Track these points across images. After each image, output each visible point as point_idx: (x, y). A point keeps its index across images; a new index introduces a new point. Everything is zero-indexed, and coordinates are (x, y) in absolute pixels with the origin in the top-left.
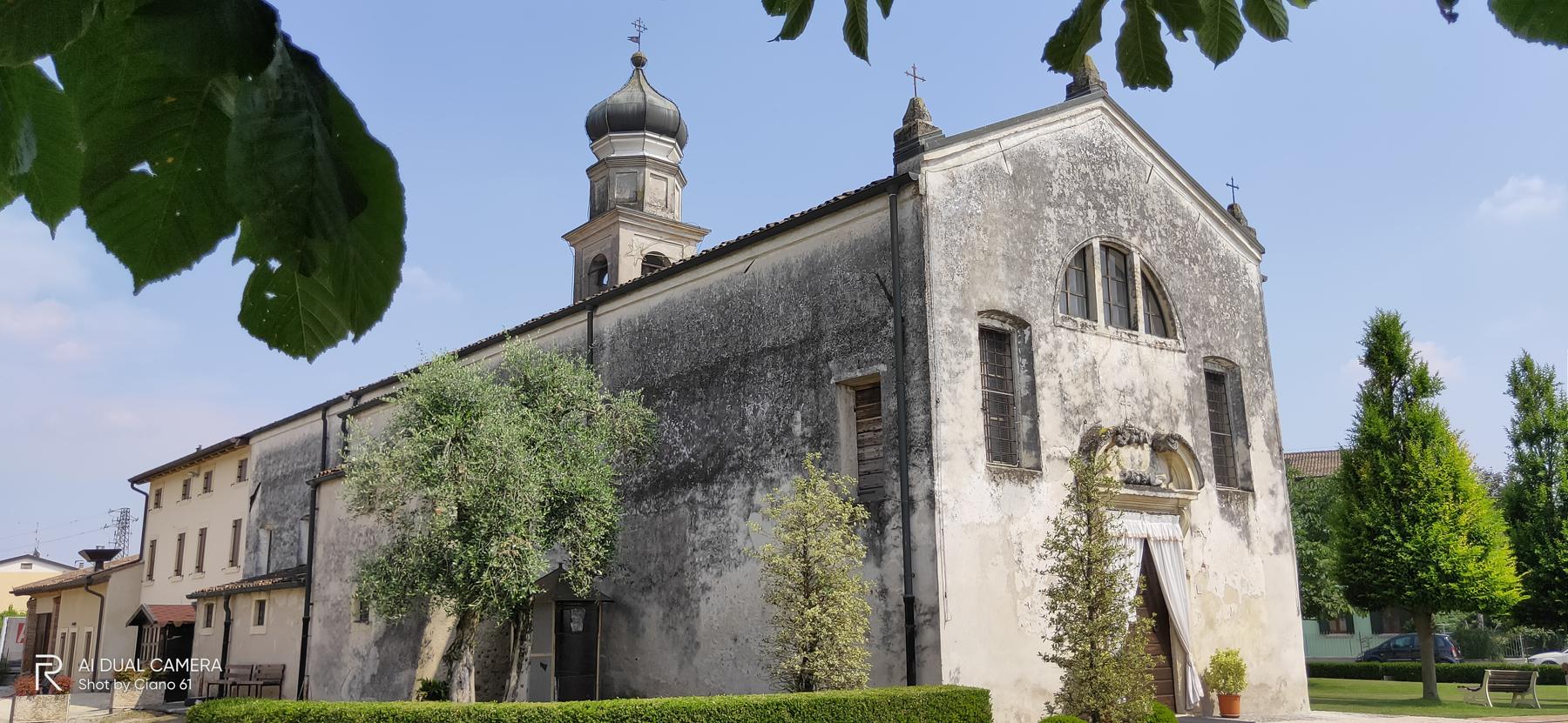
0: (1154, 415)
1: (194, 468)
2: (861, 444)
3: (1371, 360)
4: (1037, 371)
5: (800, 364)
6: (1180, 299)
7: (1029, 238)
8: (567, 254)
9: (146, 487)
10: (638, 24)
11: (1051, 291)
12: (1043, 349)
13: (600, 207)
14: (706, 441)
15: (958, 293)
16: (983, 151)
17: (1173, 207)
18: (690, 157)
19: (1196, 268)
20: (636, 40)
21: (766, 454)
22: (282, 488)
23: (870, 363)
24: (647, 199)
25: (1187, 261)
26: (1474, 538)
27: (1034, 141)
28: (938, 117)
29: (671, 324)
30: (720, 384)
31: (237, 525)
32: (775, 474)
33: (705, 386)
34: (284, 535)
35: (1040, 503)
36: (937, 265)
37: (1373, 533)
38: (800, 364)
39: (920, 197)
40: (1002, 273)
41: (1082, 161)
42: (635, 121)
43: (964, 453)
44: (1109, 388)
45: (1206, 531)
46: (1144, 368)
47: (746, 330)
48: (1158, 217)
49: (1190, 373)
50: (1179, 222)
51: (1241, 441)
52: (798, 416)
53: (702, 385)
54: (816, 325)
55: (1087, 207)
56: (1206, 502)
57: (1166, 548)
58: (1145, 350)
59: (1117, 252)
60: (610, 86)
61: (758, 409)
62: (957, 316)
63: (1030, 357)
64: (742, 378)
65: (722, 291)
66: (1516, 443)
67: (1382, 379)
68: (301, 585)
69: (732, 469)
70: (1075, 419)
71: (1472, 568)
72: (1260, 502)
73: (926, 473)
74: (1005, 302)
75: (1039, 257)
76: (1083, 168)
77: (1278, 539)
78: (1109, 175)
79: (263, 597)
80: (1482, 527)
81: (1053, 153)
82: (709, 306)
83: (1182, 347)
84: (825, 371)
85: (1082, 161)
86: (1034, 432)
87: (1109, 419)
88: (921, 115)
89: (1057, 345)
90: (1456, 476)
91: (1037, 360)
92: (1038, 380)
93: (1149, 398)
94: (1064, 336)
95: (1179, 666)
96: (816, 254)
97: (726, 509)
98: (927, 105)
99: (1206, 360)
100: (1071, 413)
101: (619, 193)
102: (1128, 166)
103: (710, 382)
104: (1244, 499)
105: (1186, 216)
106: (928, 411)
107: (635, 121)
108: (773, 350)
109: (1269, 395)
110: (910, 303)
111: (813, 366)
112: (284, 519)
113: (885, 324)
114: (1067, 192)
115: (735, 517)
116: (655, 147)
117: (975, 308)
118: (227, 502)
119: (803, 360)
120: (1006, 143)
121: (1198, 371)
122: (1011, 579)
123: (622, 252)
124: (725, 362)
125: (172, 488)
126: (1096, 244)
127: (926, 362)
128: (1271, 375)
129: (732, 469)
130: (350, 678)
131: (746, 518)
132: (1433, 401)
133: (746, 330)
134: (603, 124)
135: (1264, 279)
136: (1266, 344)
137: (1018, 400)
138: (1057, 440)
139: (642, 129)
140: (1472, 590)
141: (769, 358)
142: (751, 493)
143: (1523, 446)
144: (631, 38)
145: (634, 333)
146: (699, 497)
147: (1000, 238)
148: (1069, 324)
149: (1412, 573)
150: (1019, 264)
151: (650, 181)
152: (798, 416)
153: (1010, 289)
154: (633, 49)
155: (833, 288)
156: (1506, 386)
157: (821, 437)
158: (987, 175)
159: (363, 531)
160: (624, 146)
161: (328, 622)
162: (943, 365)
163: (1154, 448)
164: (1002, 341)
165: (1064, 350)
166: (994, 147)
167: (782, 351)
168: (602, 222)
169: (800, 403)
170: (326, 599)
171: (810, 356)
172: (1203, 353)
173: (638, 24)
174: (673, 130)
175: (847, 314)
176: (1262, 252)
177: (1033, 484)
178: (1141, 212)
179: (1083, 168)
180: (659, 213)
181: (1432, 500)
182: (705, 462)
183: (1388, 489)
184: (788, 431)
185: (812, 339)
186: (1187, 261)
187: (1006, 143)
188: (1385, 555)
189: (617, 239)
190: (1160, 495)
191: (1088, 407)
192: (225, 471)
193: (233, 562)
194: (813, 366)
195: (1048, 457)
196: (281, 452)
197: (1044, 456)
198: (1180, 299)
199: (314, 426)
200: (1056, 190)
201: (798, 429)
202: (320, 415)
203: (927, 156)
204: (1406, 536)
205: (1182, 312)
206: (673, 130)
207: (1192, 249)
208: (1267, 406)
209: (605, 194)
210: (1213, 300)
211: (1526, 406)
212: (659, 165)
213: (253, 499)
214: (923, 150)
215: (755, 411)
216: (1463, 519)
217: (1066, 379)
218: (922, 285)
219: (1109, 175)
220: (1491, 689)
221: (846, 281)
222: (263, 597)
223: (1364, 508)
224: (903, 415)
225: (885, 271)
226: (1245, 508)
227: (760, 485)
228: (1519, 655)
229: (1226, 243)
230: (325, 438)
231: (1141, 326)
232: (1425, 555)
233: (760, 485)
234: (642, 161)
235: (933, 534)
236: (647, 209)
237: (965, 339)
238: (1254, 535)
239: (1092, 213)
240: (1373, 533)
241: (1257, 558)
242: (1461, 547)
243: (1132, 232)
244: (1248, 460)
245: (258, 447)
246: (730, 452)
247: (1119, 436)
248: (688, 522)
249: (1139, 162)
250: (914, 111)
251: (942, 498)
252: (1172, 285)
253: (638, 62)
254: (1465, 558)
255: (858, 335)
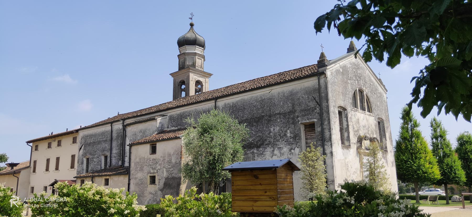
1: (53, 139)
2: (306, 139)
3: (403, 118)
5: (289, 118)
7: (345, 88)
8: (171, 79)
9: (31, 144)
10: (192, 14)
12: (349, 116)
13: (182, 67)
14: (257, 137)
16: (336, 66)
17: (370, 80)
18: (207, 52)
20: (191, 19)
21: (278, 141)
22: (93, 146)
23: (312, 119)
24: (196, 65)
26: (430, 163)
28: (328, 57)
29: (244, 105)
30: (262, 122)
31: (73, 157)
32: (281, 146)
33: (257, 122)
34: (94, 160)
36: (330, 95)
37: (406, 162)
38: (289, 118)
39: (326, 77)
40: (341, 97)
42: (194, 42)
46: (367, 121)
47: (270, 109)
49: (375, 122)
50: (372, 84)
52: (289, 131)
53: (255, 122)
54: (293, 108)
58: (367, 116)
59: (361, 92)
60: (183, 31)
61: (275, 129)
63: (347, 118)
64: (269, 121)
65: (261, 97)
66: (432, 139)
67: (406, 123)
68: (127, 174)
69: (266, 144)
70: (356, 133)
71: (430, 171)
73: (330, 147)
74: (342, 105)
76: (354, 70)
78: (359, 72)
79: (107, 177)
80: (431, 160)
82: (256, 101)
84: (297, 120)
86: (348, 137)
87: (362, 134)
88: (325, 57)
89: (352, 115)
90: (425, 147)
91: (349, 118)
94: (353, 113)
96: (293, 90)
97: (265, 155)
98: (326, 54)
101: (188, 63)
103: (258, 121)
104: (386, 153)
105: (373, 82)
106: (330, 131)
107: (194, 42)
108: (279, 114)
110: (324, 104)
111: (293, 119)
112: (94, 155)
113: (316, 109)
115: (268, 157)
116: (198, 50)
117: (337, 106)
118: (69, 149)
119: (289, 117)
120: (341, 64)
122: (346, 173)
123: (190, 80)
124: (263, 116)
125: (43, 146)
127: (329, 119)
129: (266, 144)
130: (148, 200)
131: (272, 157)
132: (418, 129)
133: (270, 109)
134: (182, 43)
137: (344, 129)
138: (354, 140)
139: (195, 45)
140: (430, 176)
141: (278, 116)
142: (273, 151)
143: (434, 140)
145: (231, 107)
146: (255, 151)
148: (353, 110)
149: (416, 172)
150: (344, 94)
151: (197, 60)
152: (289, 131)
154: (190, 21)
155: (299, 99)
156: (430, 125)
157: (296, 137)
158: (338, 71)
159: (151, 159)
160: (189, 49)
161: (137, 184)
163: (370, 141)
167: (284, 114)
168: (183, 71)
169: (289, 128)
170: (136, 178)
171: (292, 116)
173: (192, 14)
174: (202, 45)
175: (304, 106)
178: (365, 81)
179: (354, 70)
180: (199, 69)
181: (420, 154)
182: (257, 142)
183: (409, 151)
184: (285, 135)
185: (293, 112)
188: (409, 167)
189: (189, 76)
191: (358, 131)
192: (66, 142)
193: (72, 167)
194: (293, 119)
196: (92, 135)
199: (108, 128)
201: (289, 135)
202: (110, 125)
203: (328, 67)
204: (414, 162)
206: (202, 45)
207: (374, 91)
209: (184, 62)
210: (378, 104)
211: (435, 130)
212: (200, 55)
213: (81, 149)
214: (327, 66)
215: (274, 130)
216: (428, 158)
217: (354, 124)
218: (327, 100)
219: (359, 72)
220: (430, 200)
221: (303, 97)
222: (107, 177)
223: (404, 155)
224: (322, 132)
225: (316, 96)
227: (276, 149)
228: (410, 193)
229: (380, 90)
230: (112, 131)
231: (366, 110)
232: (419, 166)
233: (276, 149)
234: (195, 54)
235: (332, 162)
236: (196, 68)
237: (336, 113)
239: (356, 81)
240: (406, 162)
241: (389, 168)
242: (427, 165)
244: (386, 144)
245: (81, 134)
246: (266, 140)
247: (365, 138)
248: (252, 158)
250: (322, 55)
251: (334, 153)
252: (371, 100)
253: (192, 25)
254: (428, 168)
255: (308, 111)
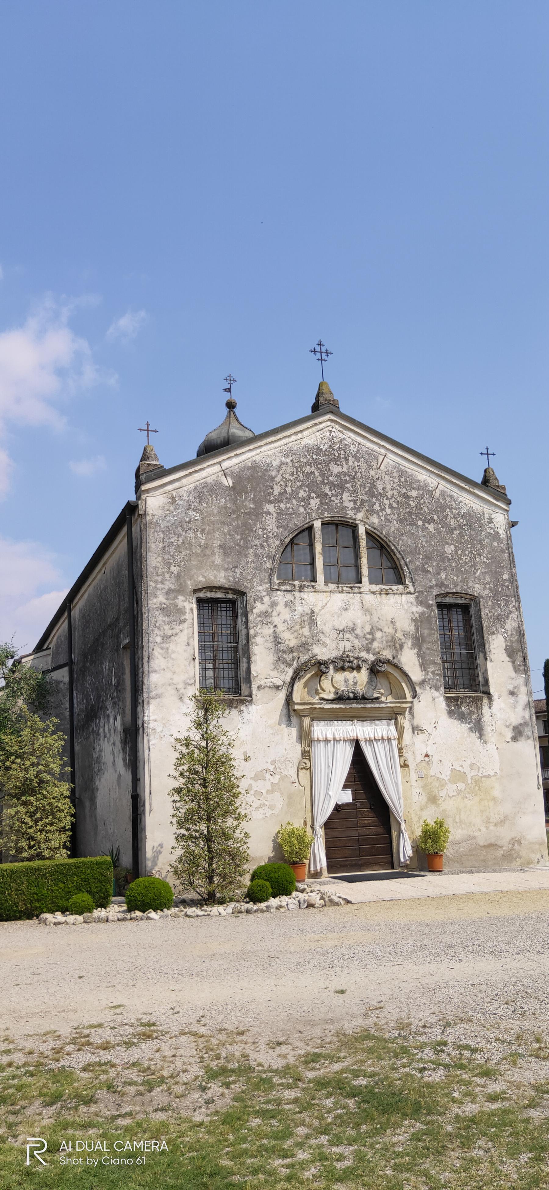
0: (375, 645)
4: (251, 625)
6: (411, 553)
7: (246, 530)
11: (268, 565)
15: (173, 580)
17: (406, 481)
19: (431, 527)
25: (420, 523)
27: (257, 458)
35: (249, 721)
41: (307, 464)
43: (173, 692)
44: (327, 629)
45: (430, 729)
46: (366, 611)
48: (389, 494)
51: (481, 655)
55: (310, 497)
56: (430, 706)
57: (380, 747)
58: (369, 599)
62: (172, 596)
70: (288, 657)
72: (497, 703)
74: (221, 578)
75: (257, 542)
76: (308, 469)
77: (518, 733)
81: (276, 463)
83: (411, 589)
85: (307, 464)
89: (273, 604)
91: (251, 617)
92: (252, 632)
93: (371, 633)
95: (394, 833)
99: (437, 596)
100: (281, 654)
102: (358, 460)
104: (477, 701)
109: (514, 616)
114: (289, 490)
117: (190, 585)
120: (225, 465)
121: (429, 606)
126: (317, 524)
128: (518, 598)
135: (513, 524)
136: (513, 576)
144: (225, 390)
147: (217, 534)
153: (226, 570)
154: (227, 397)
162: (156, 631)
164: (223, 609)
165: (280, 608)
166: (217, 468)
172: (435, 592)
176: (509, 502)
177: (243, 707)
186: (420, 523)
187: (225, 465)
190: (383, 705)
191: (304, 646)
195: (259, 687)
197: (254, 686)
198: (411, 553)
200: (277, 490)
205: (410, 564)
208: (510, 625)
217: (281, 627)
226: (479, 708)
231: (365, 579)
238: (488, 729)
241: (491, 747)
243: (358, 510)
244: (486, 670)
249: (371, 454)
253: (231, 406)
